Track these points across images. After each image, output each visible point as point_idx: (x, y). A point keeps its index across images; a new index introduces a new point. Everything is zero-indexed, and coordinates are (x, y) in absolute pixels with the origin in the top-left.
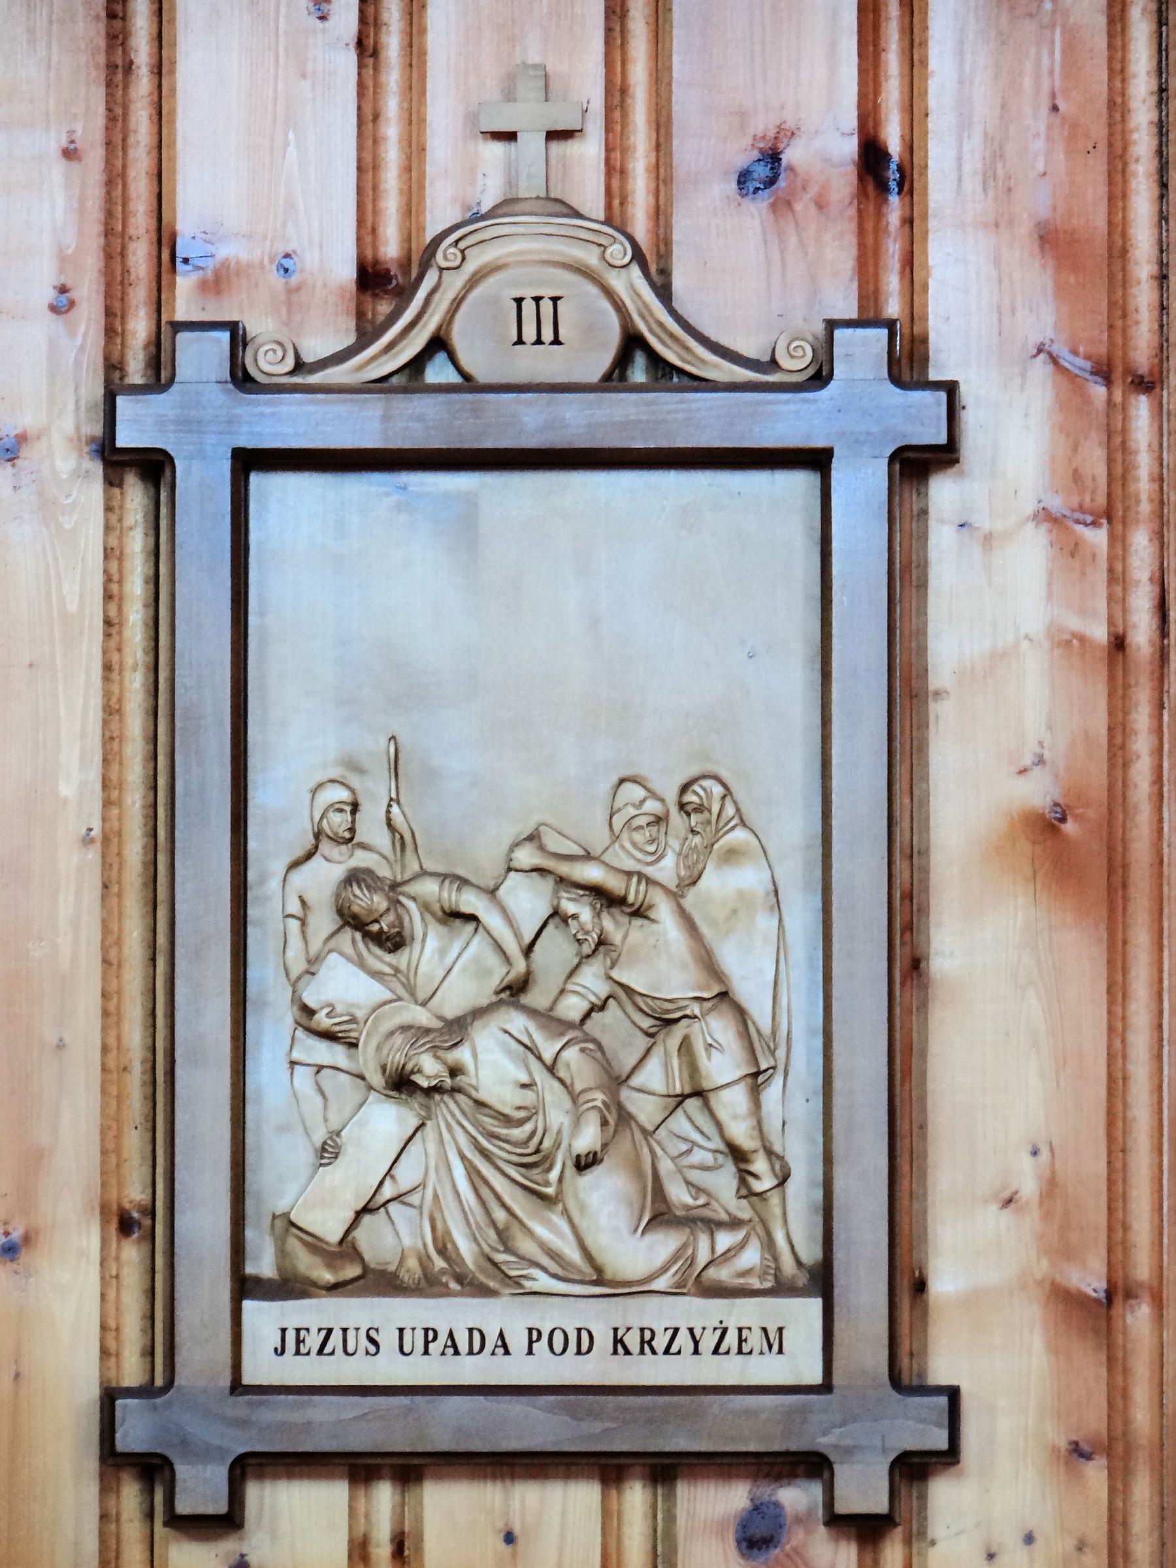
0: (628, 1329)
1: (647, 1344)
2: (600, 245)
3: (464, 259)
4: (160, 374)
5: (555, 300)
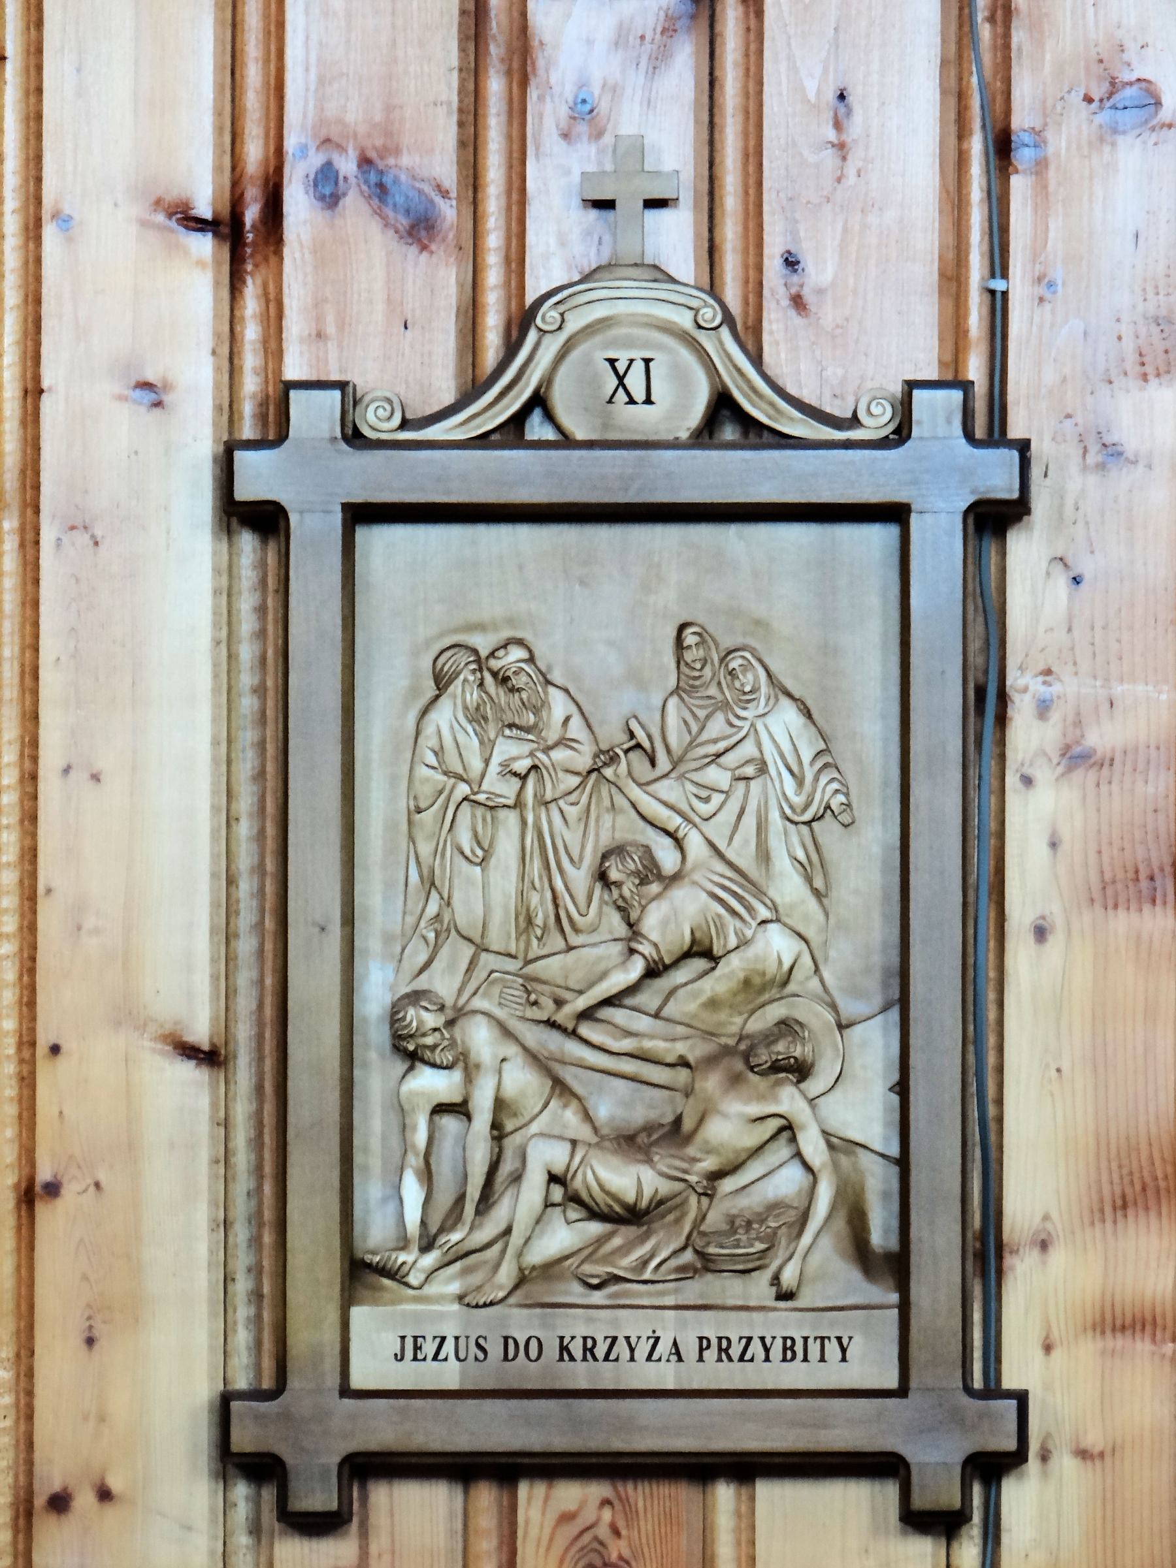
0: (573, 1338)
1: (724, 1351)
2: (691, 308)
3: (563, 321)
4: (276, 428)
5: (647, 361)
